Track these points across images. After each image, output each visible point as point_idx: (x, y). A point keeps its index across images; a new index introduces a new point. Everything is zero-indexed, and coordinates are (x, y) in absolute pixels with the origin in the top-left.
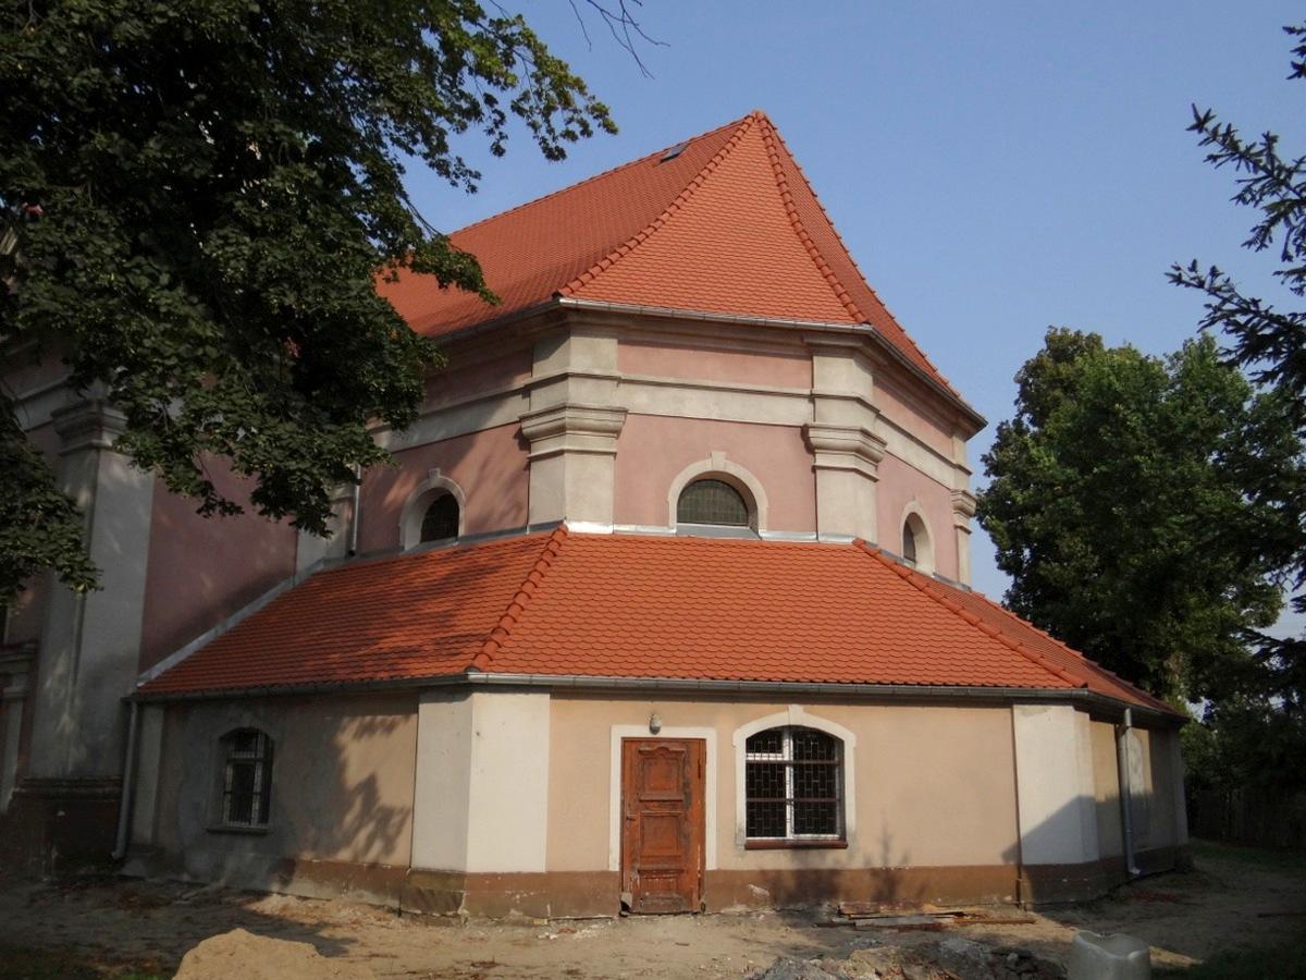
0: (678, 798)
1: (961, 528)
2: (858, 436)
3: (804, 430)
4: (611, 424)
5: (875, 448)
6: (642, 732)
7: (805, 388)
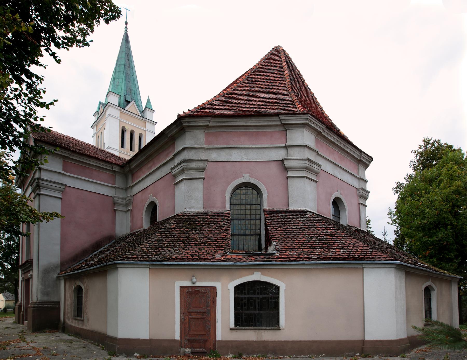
0: (204, 311)
1: (362, 204)
2: (307, 162)
3: (283, 161)
4: (201, 166)
5: (315, 168)
6: (188, 284)
7: (283, 144)
